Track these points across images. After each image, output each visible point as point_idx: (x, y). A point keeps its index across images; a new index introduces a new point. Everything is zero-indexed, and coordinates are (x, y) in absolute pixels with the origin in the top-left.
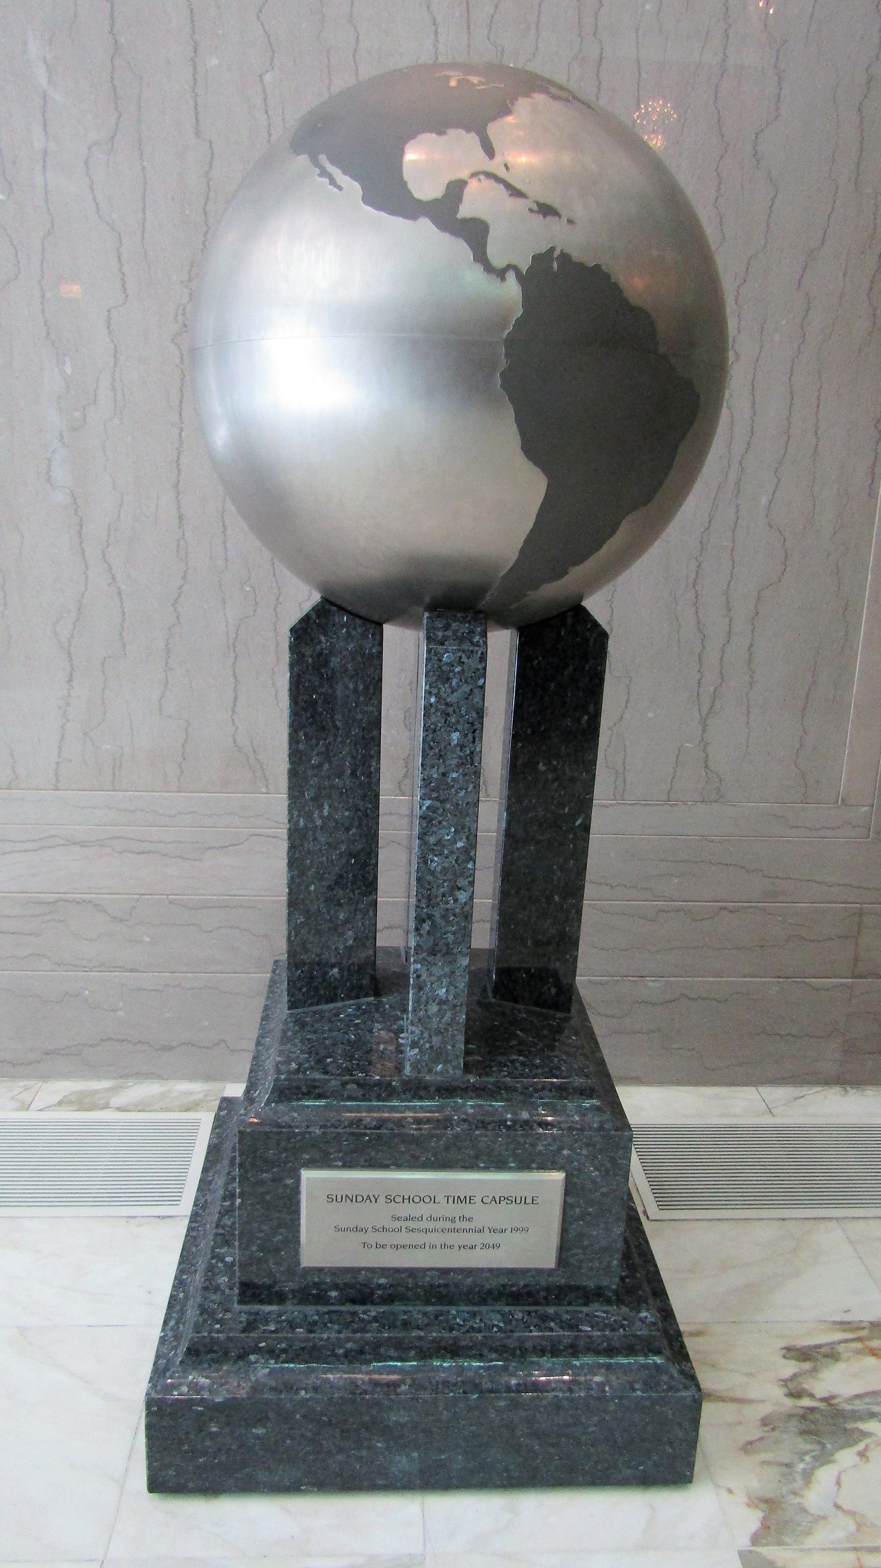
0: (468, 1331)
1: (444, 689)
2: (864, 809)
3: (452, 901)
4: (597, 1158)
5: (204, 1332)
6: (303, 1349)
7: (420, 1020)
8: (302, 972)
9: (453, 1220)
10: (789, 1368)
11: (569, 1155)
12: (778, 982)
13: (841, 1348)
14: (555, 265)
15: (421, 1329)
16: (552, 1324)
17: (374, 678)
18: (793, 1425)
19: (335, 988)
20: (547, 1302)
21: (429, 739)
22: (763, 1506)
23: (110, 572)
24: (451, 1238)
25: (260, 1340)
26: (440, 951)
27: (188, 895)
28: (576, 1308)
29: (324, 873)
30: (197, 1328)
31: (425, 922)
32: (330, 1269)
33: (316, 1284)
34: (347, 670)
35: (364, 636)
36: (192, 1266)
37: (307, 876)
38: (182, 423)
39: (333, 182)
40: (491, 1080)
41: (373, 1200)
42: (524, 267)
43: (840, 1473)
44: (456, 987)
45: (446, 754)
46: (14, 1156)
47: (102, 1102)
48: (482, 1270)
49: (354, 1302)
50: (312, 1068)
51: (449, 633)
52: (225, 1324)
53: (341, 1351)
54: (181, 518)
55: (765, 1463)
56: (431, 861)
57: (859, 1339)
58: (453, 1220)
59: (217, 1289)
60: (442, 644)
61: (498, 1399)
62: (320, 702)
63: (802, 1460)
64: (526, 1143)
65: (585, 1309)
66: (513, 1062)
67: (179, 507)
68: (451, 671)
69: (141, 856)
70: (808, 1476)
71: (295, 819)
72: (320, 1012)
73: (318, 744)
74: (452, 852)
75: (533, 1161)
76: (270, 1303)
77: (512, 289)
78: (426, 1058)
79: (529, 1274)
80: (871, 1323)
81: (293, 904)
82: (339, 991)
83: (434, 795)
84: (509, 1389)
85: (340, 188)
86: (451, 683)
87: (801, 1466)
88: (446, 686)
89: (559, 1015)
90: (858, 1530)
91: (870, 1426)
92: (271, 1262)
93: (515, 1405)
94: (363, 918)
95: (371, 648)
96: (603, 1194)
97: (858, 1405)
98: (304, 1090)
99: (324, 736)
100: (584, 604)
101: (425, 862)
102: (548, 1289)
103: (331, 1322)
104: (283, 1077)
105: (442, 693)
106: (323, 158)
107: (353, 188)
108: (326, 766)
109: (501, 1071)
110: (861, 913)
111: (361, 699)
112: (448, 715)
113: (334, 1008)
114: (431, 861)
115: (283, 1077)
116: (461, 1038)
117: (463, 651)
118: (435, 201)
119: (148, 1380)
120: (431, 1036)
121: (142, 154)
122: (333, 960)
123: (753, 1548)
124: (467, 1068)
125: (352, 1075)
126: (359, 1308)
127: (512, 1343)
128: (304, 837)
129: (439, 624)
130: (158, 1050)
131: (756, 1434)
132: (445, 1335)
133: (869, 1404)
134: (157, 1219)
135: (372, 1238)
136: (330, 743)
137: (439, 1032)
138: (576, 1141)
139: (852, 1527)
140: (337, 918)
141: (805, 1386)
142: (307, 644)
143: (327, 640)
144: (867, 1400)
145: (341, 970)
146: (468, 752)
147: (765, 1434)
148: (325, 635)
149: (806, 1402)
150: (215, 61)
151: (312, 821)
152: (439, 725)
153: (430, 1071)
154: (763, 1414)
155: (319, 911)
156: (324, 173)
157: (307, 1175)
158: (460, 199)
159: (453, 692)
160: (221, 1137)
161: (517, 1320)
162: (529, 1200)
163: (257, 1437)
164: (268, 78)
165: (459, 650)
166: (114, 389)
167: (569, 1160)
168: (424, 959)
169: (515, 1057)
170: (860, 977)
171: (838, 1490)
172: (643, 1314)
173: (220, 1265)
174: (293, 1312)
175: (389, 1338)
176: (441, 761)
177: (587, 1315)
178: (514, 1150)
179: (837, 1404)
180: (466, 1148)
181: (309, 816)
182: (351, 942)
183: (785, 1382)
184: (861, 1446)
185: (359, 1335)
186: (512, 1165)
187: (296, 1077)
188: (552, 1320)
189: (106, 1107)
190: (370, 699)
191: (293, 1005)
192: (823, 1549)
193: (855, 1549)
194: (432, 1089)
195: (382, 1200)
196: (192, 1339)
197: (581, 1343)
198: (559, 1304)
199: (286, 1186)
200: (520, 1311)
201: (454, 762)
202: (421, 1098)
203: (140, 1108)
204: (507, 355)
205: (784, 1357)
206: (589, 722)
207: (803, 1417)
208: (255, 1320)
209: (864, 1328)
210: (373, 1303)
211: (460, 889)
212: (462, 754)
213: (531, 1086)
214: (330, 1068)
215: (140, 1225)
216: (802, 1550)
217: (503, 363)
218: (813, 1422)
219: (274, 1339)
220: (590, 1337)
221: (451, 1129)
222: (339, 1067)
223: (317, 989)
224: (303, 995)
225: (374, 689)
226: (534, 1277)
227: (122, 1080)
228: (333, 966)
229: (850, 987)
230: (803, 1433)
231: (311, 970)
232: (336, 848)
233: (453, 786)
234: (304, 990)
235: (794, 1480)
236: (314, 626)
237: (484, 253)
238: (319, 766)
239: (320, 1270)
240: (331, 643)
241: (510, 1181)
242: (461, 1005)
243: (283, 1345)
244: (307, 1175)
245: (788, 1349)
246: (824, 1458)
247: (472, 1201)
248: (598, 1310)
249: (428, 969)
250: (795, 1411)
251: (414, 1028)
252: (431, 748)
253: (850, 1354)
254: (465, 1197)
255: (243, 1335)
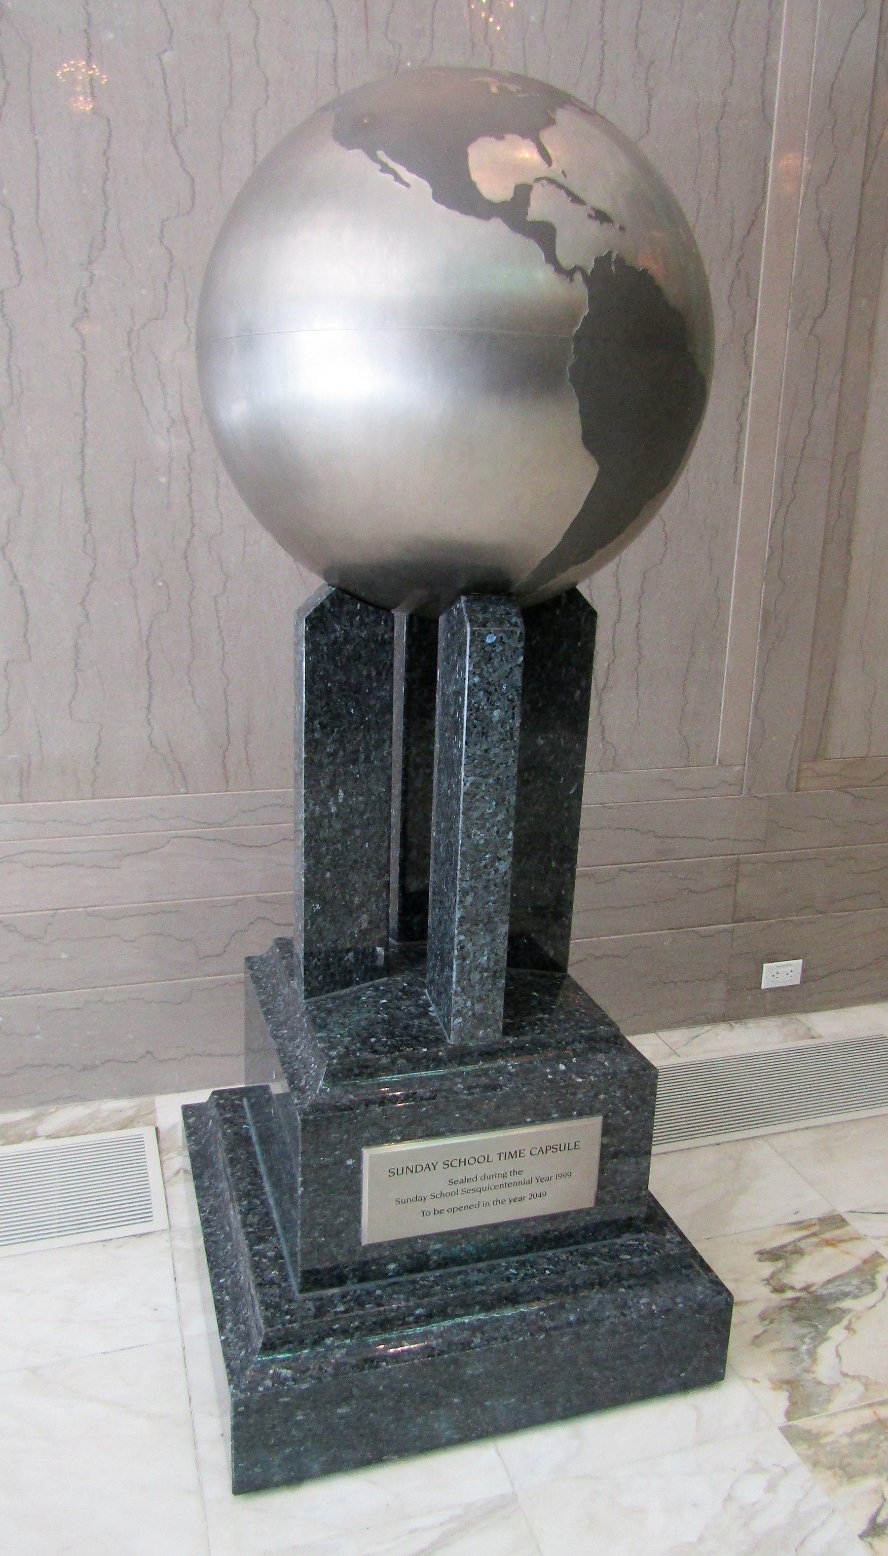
0: (523, 1279)
1: (487, 669)
2: (738, 768)
3: (493, 872)
4: (629, 1097)
5: (277, 1325)
6: (375, 1323)
7: (463, 989)
8: (319, 960)
9: (504, 1176)
10: (767, 1269)
11: (605, 1098)
12: (671, 934)
13: (802, 1244)
14: (613, 267)
15: (482, 1284)
16: (595, 1258)
17: (386, 664)
18: (786, 1314)
19: (351, 972)
20: (586, 1239)
21: (472, 717)
22: (785, 1386)
23: (12, 570)
24: (502, 1194)
25: (334, 1321)
26: (481, 921)
27: (107, 905)
28: (610, 1241)
29: (339, 860)
30: (269, 1322)
31: (468, 895)
32: (389, 1242)
33: (374, 1261)
34: (360, 656)
35: (377, 622)
36: (226, 1268)
37: (322, 864)
38: (85, 411)
39: (398, 178)
40: (527, 1038)
41: (432, 1167)
42: (590, 267)
43: (837, 1348)
44: (496, 954)
45: (487, 731)
46: (103, 1170)
47: (28, 1132)
48: (527, 1220)
49: (411, 1271)
50: (360, 1049)
51: (488, 616)
52: (294, 1314)
53: (411, 1319)
54: (87, 511)
55: (774, 1351)
56: (475, 835)
57: (814, 1234)
58: (504, 1176)
59: (272, 1283)
60: (484, 625)
61: (563, 1335)
62: (335, 690)
63: (804, 1343)
64: (567, 1093)
65: (619, 1241)
66: (541, 1019)
67: (85, 501)
68: (493, 651)
69: (55, 868)
70: (812, 1353)
71: (311, 807)
72: (339, 997)
73: (333, 732)
74: (493, 826)
75: (574, 1110)
76: (332, 1286)
77: (580, 290)
78: (469, 1025)
79: (570, 1216)
80: (819, 1219)
81: (310, 893)
82: (355, 975)
83: (478, 771)
84: (570, 1324)
85: (407, 185)
86: (493, 663)
87: (804, 1347)
88: (489, 665)
89: (557, 975)
90: (866, 1389)
91: (846, 1304)
92: (332, 1245)
93: (578, 1337)
94: (376, 901)
95: (383, 636)
96: (634, 1131)
97: (831, 1289)
98: (356, 1071)
99: (338, 723)
100: (577, 587)
101: (469, 837)
102: (586, 1229)
103: (396, 1293)
104: (335, 1061)
105: (484, 673)
106: (381, 154)
107: (421, 187)
108: (341, 753)
109: (533, 1030)
110: (738, 863)
111: (375, 685)
112: (490, 693)
113: (351, 992)
114: (475, 835)
115: (335, 1061)
116: (500, 1003)
117: (504, 632)
118: (503, 203)
119: (227, 1384)
120: (473, 1004)
121: (34, 128)
122: (349, 946)
123: (790, 1423)
124: (506, 1032)
125: (399, 1051)
126: (417, 1276)
127: (565, 1282)
128: (320, 826)
129: (477, 607)
130: (80, 1071)
131: (759, 1329)
132: (504, 1285)
133: (840, 1286)
134: (134, 1239)
135: (430, 1205)
136: (344, 730)
137: (480, 999)
138: (610, 1085)
139: (861, 1388)
140: (352, 902)
141: (785, 1281)
142: (322, 633)
143: (341, 629)
144: (837, 1283)
145: (356, 953)
146: (508, 728)
147: (766, 1327)
148: (339, 624)
149: (790, 1294)
150: (111, 36)
151: (328, 809)
152: (482, 704)
153: (472, 1037)
154: (758, 1312)
155: (335, 898)
156: (385, 169)
157: (367, 1153)
158: (527, 202)
159: (494, 672)
160: (200, 1143)
161: (563, 1261)
162: (572, 1146)
163: (342, 1417)
164: (166, 57)
165: (500, 631)
166: (10, 376)
167: (605, 1102)
168: (468, 930)
169: (540, 1016)
170: (739, 921)
171: (840, 1360)
172: (668, 1237)
173: (264, 1261)
174: (355, 1291)
175: (454, 1297)
176: (484, 738)
177: (622, 1245)
178: (557, 1101)
179: (815, 1291)
180: (515, 1105)
181: (324, 803)
182: (365, 925)
183: (768, 1281)
184: (845, 1322)
185: (426, 1300)
186: (555, 1116)
187: (348, 1060)
188: (594, 1255)
189: (34, 1136)
190: (383, 685)
191: (310, 993)
192: (845, 1411)
193: (870, 1405)
194: (476, 1055)
195: (440, 1166)
196: (267, 1334)
197: (625, 1271)
198: (594, 1240)
199: (348, 1167)
200: (562, 1253)
201: (496, 738)
202: (466, 1064)
203: (73, 1132)
204: (575, 352)
205: (760, 1261)
206: (582, 696)
207: (792, 1307)
208: (322, 1306)
209: (814, 1225)
210: (429, 1269)
211: (500, 859)
212: (502, 730)
213: (563, 1040)
214: (377, 1047)
215: (118, 1247)
216: (827, 1416)
217: (572, 360)
218: (802, 1310)
219: (346, 1319)
220: (631, 1264)
221: (501, 1090)
222: (385, 1045)
223: (332, 975)
224: (319, 982)
225: (387, 675)
226: (573, 1218)
227: (40, 1108)
228: (349, 950)
229: (732, 931)
230: (797, 1320)
231: (327, 957)
232: (350, 834)
233: (495, 761)
234: (320, 978)
235: (803, 1360)
236: (329, 615)
237: (555, 257)
238: (334, 754)
239: (379, 1245)
240: (345, 631)
241: (535, 1133)
242: (501, 971)
243: (357, 1323)
244: (367, 1153)
245: (761, 1253)
246: (820, 1337)
247: (521, 1155)
248: (628, 1239)
249: (471, 940)
250: (783, 1304)
251: (458, 998)
252: (475, 727)
253: (812, 1248)
254: (516, 1152)
255: (317, 1321)
